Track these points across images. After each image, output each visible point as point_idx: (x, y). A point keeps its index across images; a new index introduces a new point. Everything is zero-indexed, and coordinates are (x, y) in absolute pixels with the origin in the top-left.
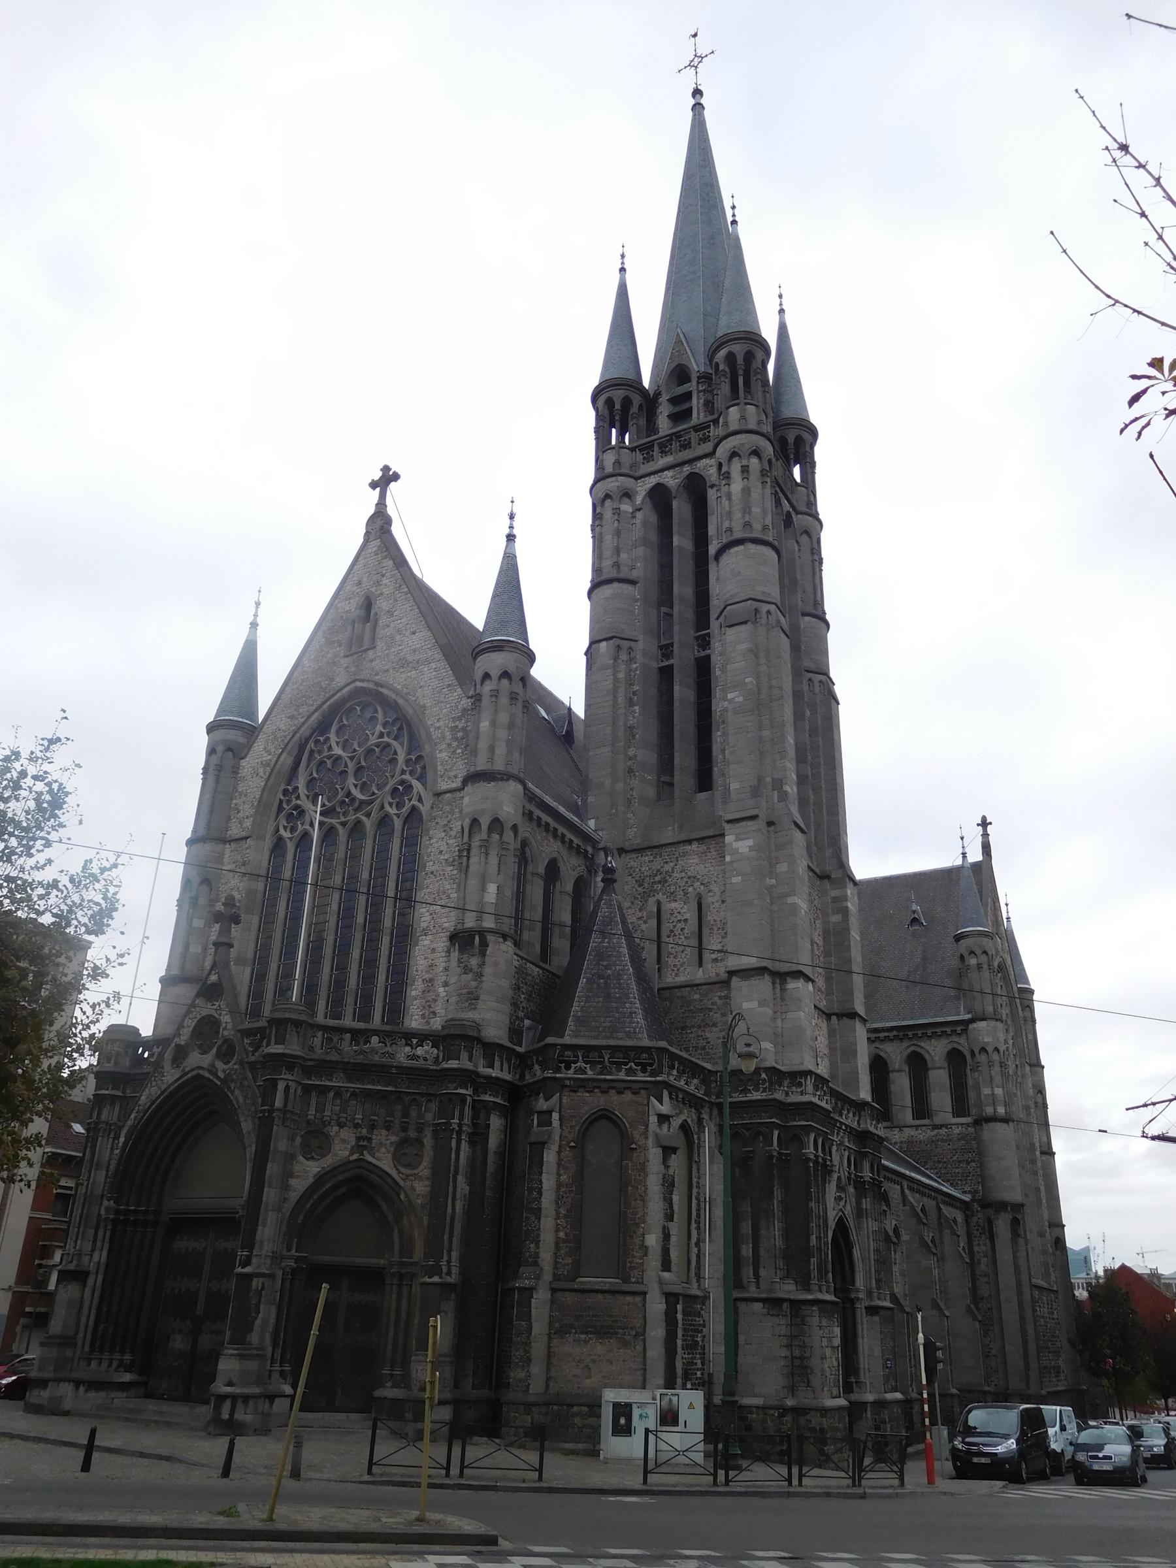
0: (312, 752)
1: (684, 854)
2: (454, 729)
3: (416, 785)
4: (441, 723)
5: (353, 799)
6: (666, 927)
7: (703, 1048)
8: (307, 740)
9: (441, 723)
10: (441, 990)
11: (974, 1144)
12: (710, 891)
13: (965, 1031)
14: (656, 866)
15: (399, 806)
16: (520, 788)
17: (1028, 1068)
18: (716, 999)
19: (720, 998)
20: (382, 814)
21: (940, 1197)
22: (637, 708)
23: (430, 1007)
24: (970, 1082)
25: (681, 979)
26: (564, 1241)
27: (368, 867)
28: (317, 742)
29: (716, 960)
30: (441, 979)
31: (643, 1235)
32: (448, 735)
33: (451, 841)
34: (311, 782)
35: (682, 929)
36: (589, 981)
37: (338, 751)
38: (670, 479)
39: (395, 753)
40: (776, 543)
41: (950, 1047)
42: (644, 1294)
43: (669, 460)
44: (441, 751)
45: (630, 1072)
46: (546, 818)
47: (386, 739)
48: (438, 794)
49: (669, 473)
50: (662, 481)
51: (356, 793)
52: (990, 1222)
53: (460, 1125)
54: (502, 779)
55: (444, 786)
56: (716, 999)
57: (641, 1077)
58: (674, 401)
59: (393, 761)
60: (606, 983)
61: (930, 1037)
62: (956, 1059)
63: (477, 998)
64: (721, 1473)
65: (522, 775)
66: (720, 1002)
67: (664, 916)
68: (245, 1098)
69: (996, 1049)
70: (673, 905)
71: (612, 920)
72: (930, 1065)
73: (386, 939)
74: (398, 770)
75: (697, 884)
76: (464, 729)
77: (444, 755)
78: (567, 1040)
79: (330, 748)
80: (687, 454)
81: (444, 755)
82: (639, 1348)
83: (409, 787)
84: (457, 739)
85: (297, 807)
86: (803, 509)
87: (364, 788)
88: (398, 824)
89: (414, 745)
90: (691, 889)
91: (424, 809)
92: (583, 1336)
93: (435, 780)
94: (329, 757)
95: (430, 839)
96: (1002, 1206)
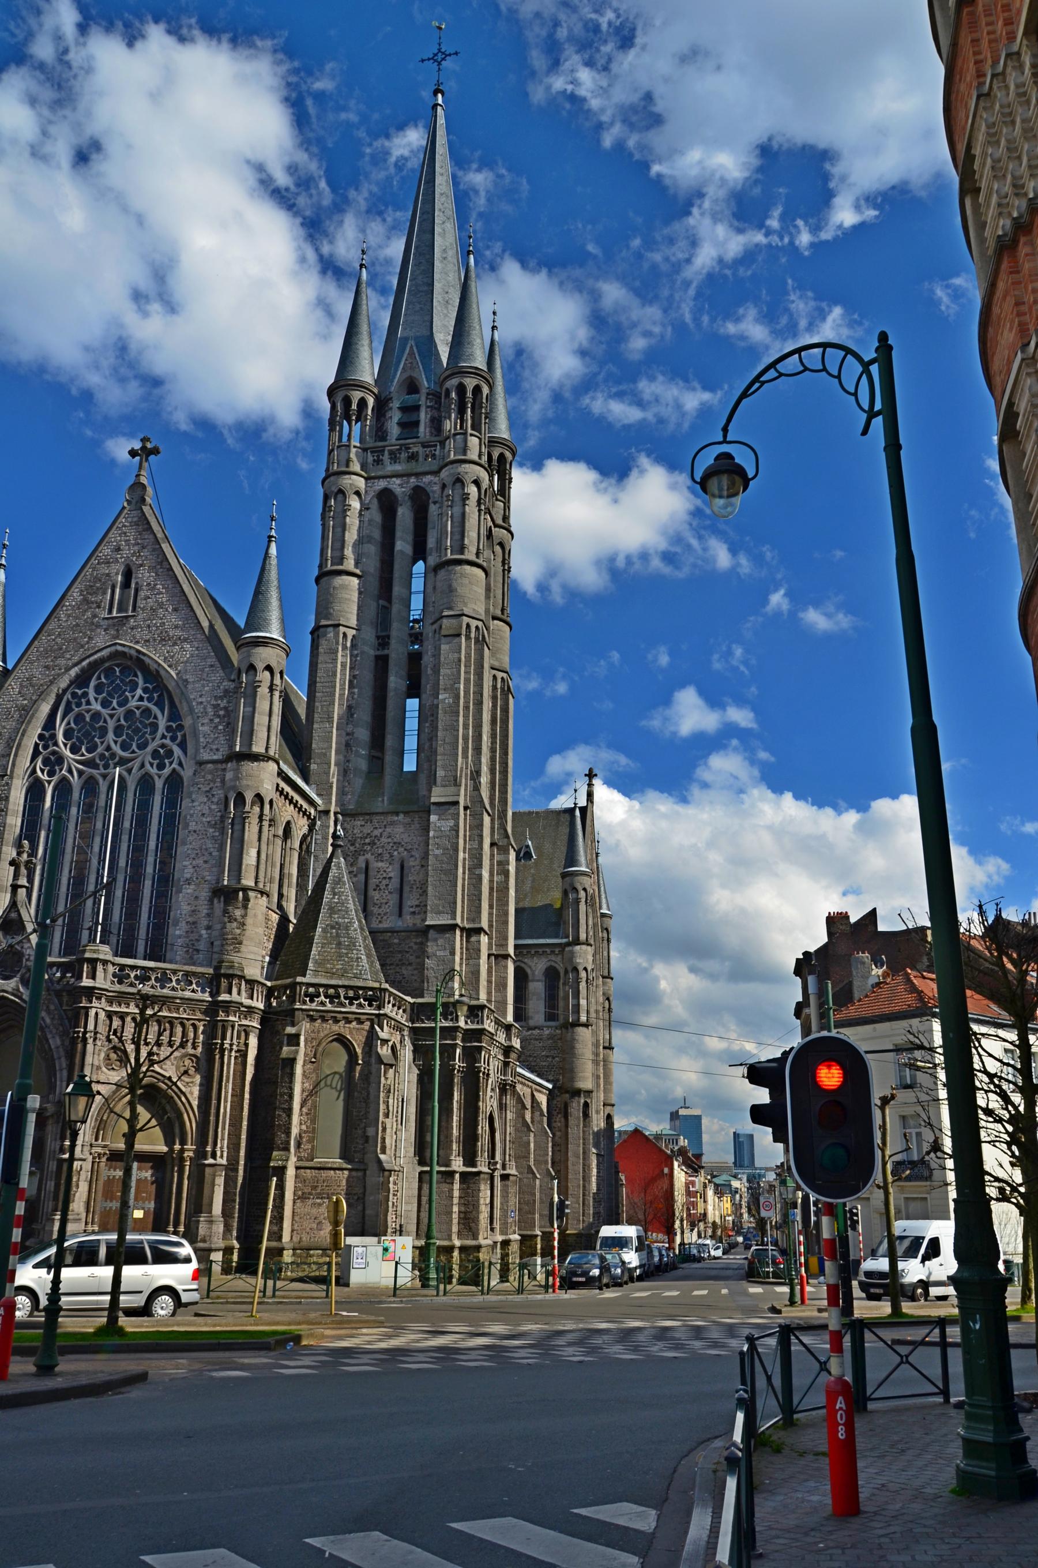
0: (68, 703)
1: (392, 823)
2: (216, 707)
3: (177, 751)
4: (203, 700)
5: (113, 755)
6: (373, 882)
7: (400, 982)
8: (65, 691)
9: (203, 700)
10: (204, 932)
11: (560, 1044)
12: (412, 856)
13: (562, 952)
14: (367, 830)
15: (161, 767)
16: (276, 767)
17: (601, 979)
18: (412, 944)
19: (416, 943)
20: (143, 771)
21: (534, 1086)
22: (356, 690)
23: (193, 945)
24: (561, 994)
25: (385, 925)
26: (305, 1132)
27: (129, 817)
28: (74, 695)
29: (414, 913)
30: (205, 922)
31: (365, 1128)
32: (210, 711)
33: (213, 807)
34: (67, 734)
35: (387, 885)
36: (324, 930)
37: (96, 706)
38: (396, 485)
39: (155, 717)
40: (485, 564)
41: (549, 964)
42: (365, 1170)
43: (398, 468)
44: (203, 724)
45: (360, 1006)
46: (301, 802)
47: (146, 703)
48: (201, 763)
49: (398, 481)
50: (390, 486)
51: (116, 749)
52: (566, 1106)
53: (231, 1045)
54: (263, 760)
55: (205, 756)
56: (412, 944)
57: (368, 1010)
58: (404, 409)
59: (155, 727)
60: (337, 933)
61: (533, 955)
62: (552, 976)
63: (240, 943)
64: (442, 1286)
65: (277, 756)
66: (415, 947)
67: (371, 873)
68: (53, 1019)
69: (585, 969)
70: (380, 864)
71: (340, 880)
72: (530, 977)
73: (148, 883)
74: (159, 734)
75: (401, 849)
76: (225, 708)
77: (206, 729)
78: (308, 979)
79: (88, 703)
80: (412, 467)
81: (206, 729)
82: (360, 1208)
83: (170, 753)
84: (219, 716)
85: (54, 753)
86: (500, 522)
87: (125, 747)
88: (159, 784)
89: (174, 715)
90: (396, 853)
91: (187, 774)
92: (318, 1201)
93: (197, 751)
94: (88, 711)
95: (193, 801)
96: (578, 1092)
